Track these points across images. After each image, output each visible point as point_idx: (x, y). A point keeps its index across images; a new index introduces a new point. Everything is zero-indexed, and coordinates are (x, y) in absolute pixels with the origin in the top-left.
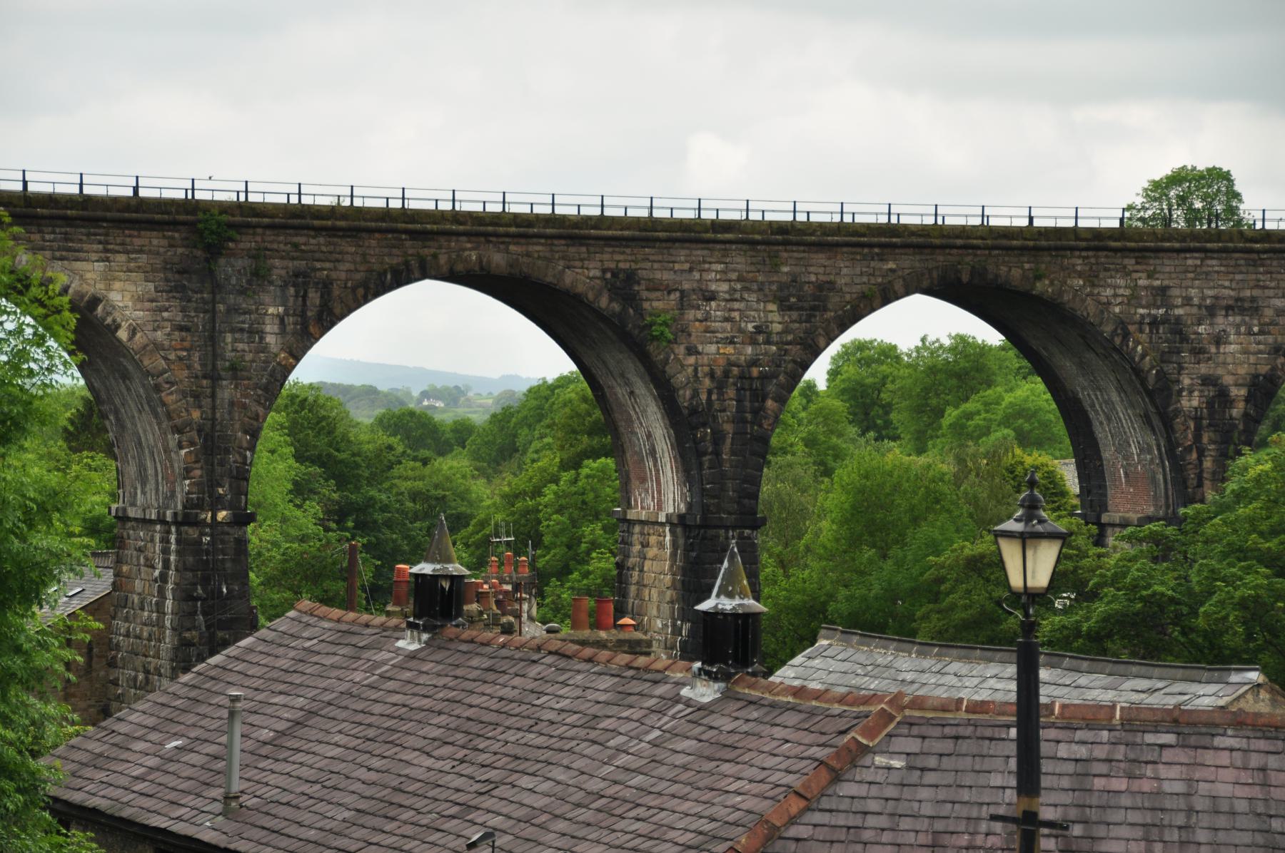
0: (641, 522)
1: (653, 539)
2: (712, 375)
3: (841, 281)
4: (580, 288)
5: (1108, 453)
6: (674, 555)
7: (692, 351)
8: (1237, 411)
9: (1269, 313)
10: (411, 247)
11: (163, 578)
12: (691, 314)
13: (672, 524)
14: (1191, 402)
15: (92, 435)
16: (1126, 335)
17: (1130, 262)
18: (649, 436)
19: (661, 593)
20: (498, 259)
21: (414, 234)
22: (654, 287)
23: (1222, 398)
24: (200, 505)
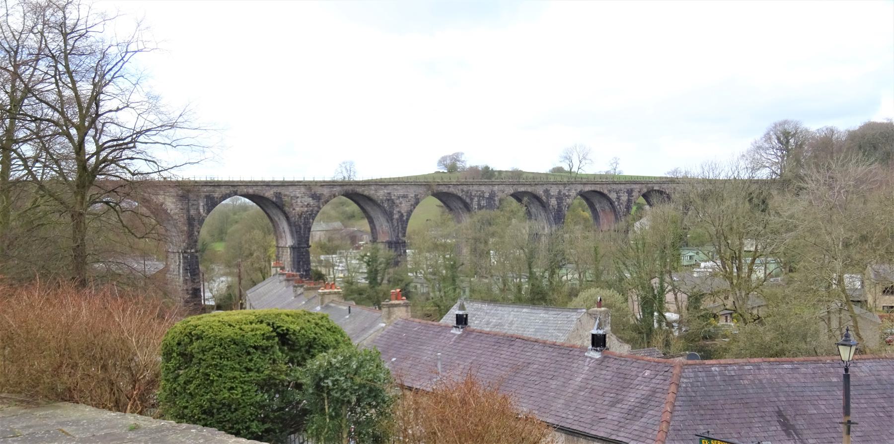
0: (282, 247)
1: (285, 251)
2: (298, 215)
3: (325, 193)
4: (269, 197)
5: (377, 228)
6: (290, 254)
7: (294, 209)
8: (405, 218)
9: (410, 198)
10: (231, 189)
11: (179, 265)
12: (293, 201)
13: (290, 248)
14: (396, 216)
15: (25, 343)
16: (383, 203)
17: (383, 187)
18: (283, 228)
19: (288, 263)
20: (251, 191)
21: (232, 186)
22: (285, 195)
23: (402, 215)
24: (187, 248)
